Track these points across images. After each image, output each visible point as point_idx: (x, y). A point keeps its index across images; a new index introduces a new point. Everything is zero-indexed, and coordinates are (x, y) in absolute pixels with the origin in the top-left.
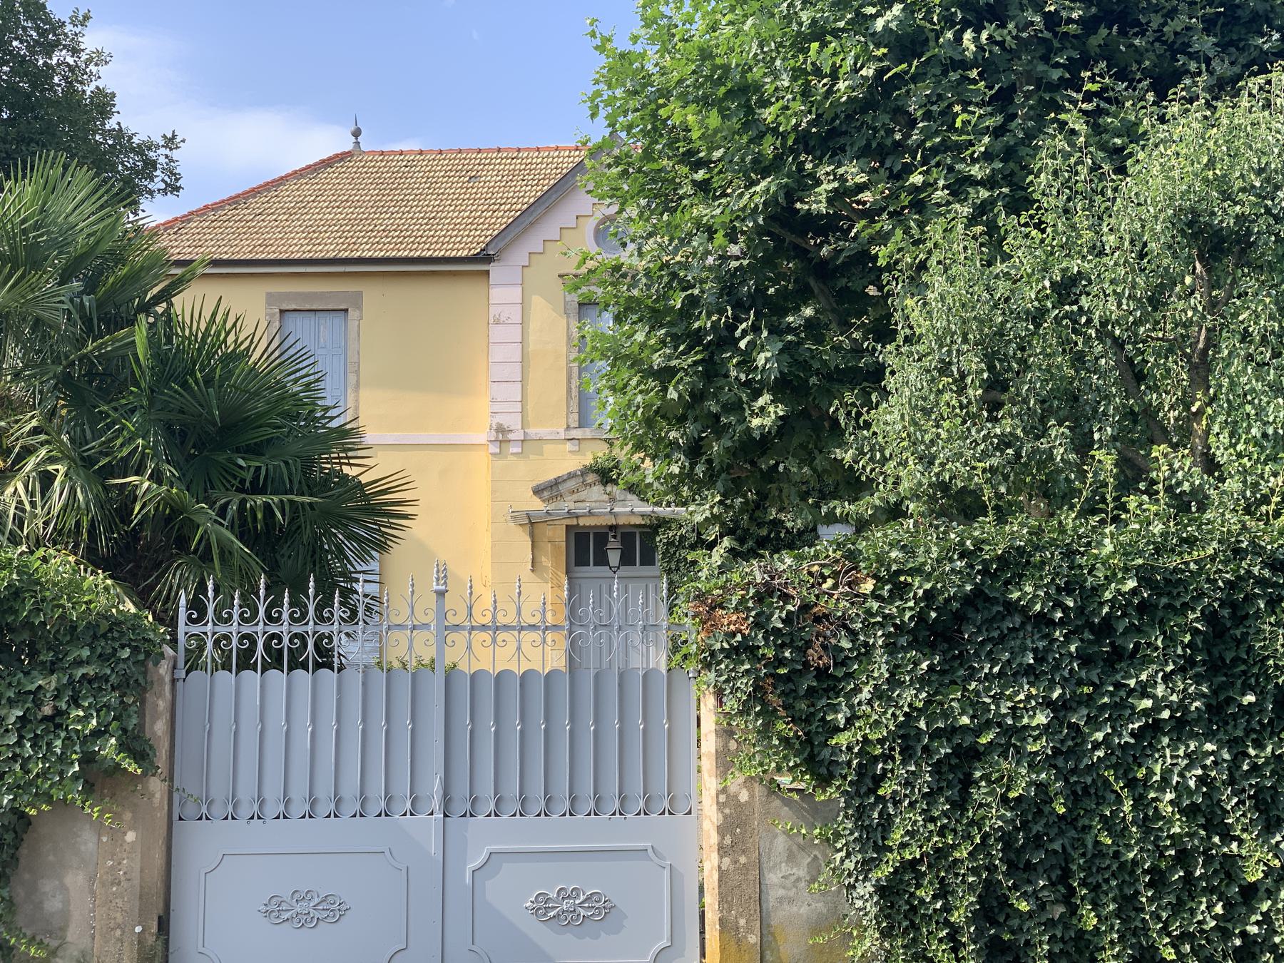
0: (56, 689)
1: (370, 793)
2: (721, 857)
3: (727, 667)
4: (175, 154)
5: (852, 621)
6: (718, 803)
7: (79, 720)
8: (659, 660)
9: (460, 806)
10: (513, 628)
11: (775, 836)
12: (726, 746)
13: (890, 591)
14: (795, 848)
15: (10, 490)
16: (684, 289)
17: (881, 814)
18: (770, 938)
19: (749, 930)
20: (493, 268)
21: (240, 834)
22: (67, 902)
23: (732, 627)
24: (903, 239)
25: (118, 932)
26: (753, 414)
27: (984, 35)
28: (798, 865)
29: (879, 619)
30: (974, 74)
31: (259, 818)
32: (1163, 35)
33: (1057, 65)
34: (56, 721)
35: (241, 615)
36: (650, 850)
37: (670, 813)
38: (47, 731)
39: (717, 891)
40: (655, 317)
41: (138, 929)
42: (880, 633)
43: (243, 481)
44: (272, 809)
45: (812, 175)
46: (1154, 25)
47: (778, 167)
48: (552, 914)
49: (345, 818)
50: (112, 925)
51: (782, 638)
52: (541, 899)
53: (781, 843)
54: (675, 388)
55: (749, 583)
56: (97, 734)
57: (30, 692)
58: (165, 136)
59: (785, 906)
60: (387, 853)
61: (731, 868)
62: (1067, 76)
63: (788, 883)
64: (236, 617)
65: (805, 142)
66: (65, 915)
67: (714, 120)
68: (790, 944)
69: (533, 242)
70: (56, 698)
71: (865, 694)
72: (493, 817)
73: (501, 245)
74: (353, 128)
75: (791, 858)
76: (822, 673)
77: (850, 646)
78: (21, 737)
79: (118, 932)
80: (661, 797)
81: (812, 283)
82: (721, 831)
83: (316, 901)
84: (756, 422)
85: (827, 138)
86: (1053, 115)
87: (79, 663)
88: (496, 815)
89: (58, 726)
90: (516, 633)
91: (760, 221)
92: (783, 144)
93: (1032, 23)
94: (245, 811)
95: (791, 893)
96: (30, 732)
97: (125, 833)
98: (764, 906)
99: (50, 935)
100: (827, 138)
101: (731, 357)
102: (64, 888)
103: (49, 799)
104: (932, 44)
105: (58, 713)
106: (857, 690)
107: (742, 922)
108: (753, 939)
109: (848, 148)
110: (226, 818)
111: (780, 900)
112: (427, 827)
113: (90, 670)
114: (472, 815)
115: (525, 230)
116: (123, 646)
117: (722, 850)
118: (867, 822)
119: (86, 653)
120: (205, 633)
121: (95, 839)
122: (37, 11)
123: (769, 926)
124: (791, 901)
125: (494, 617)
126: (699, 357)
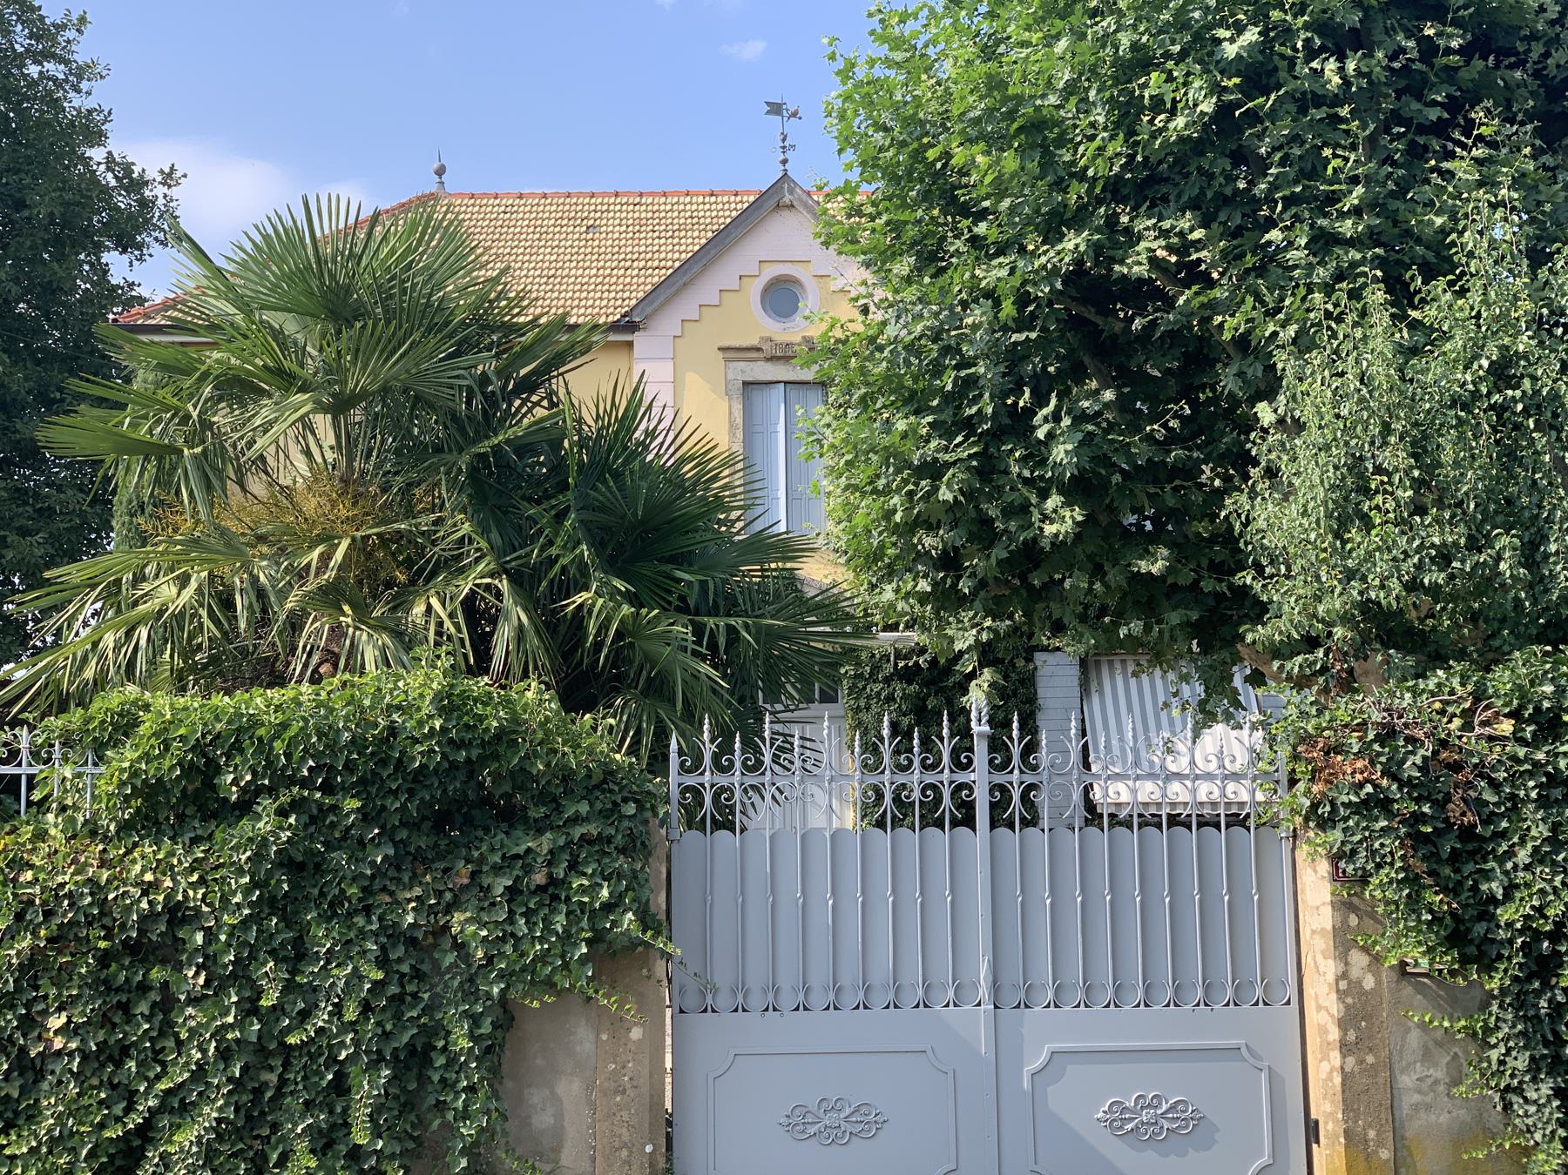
0: (551, 852)
1: (905, 980)
2: (1344, 1056)
3: (1357, 824)
4: (174, 192)
5: (1493, 769)
6: (1338, 991)
7: (583, 890)
8: (849, 818)
9: (1011, 997)
10: (1186, 777)
11: (1408, 1030)
12: (1345, 921)
13: (1534, 734)
14: (1431, 1044)
15: (419, 609)
16: (958, 367)
17: (1550, 1001)
18: (1405, 1153)
19: (1380, 1143)
20: (638, 338)
21: (758, 1029)
22: (559, 1116)
23: (1359, 777)
24: (1254, 308)
25: (624, 1153)
26: (1045, 518)
27: (1351, 66)
28: (1435, 1065)
29: (1527, 767)
30: (1344, 111)
31: (775, 1009)
32: (1545, 68)
33: (1434, 103)
34: (553, 891)
35: (923, 760)
36: (1244, 1050)
37: (1266, 1004)
38: (540, 905)
39: (1339, 1097)
40: (914, 403)
41: (649, 1149)
42: (1531, 784)
43: (682, 598)
44: (818, 999)
45: (1127, 231)
46: (1535, 56)
47: (1082, 220)
48: (1129, 1127)
49: (877, 1010)
50: (617, 1144)
51: (1419, 789)
52: (797, 1112)
53: (1414, 1037)
54: (949, 486)
55: (1364, 723)
56: (608, 907)
57: (517, 857)
58: (162, 172)
59: (1422, 1114)
60: (929, 1052)
61: (1356, 1069)
62: (1446, 115)
63: (1425, 1086)
64: (738, 764)
65: (1114, 190)
66: (558, 1132)
67: (1010, 161)
68: (1429, 1159)
69: (687, 307)
70: (550, 864)
71: (1523, 856)
72: (1052, 1008)
73: (649, 310)
74: (436, 165)
75: (1427, 1056)
76: (1467, 833)
77: (1495, 799)
78: (511, 912)
79: (624, 1153)
80: (944, 987)
81: (1087, 360)
82: (1343, 1024)
83: (848, 1111)
84: (1050, 529)
85: (1145, 186)
86: (1433, 162)
87: (576, 820)
88: (1056, 1006)
89: (555, 898)
90: (1188, 783)
91: (1059, 286)
92: (1089, 192)
93: (1403, 51)
94: (849, 1000)
95: (1428, 1099)
96: (520, 905)
97: (629, 1030)
98: (1397, 1113)
99: (546, 1152)
100: (1145, 186)
101: (1012, 451)
102: (555, 1099)
103: (549, 984)
104: (1283, 75)
105: (552, 881)
106: (1510, 854)
107: (1372, 1134)
108: (1385, 1154)
109: (1172, 197)
110: (736, 1010)
111: (1416, 1108)
112: (975, 1021)
113: (592, 829)
114: (1027, 1006)
115: (677, 293)
116: (625, 800)
117: (1345, 1048)
118: (1531, 1013)
119: (584, 808)
120: (702, 785)
121: (592, 1037)
122: (28, 13)
123: (1403, 1138)
124: (1428, 1108)
125: (1193, 762)
126: (975, 450)
